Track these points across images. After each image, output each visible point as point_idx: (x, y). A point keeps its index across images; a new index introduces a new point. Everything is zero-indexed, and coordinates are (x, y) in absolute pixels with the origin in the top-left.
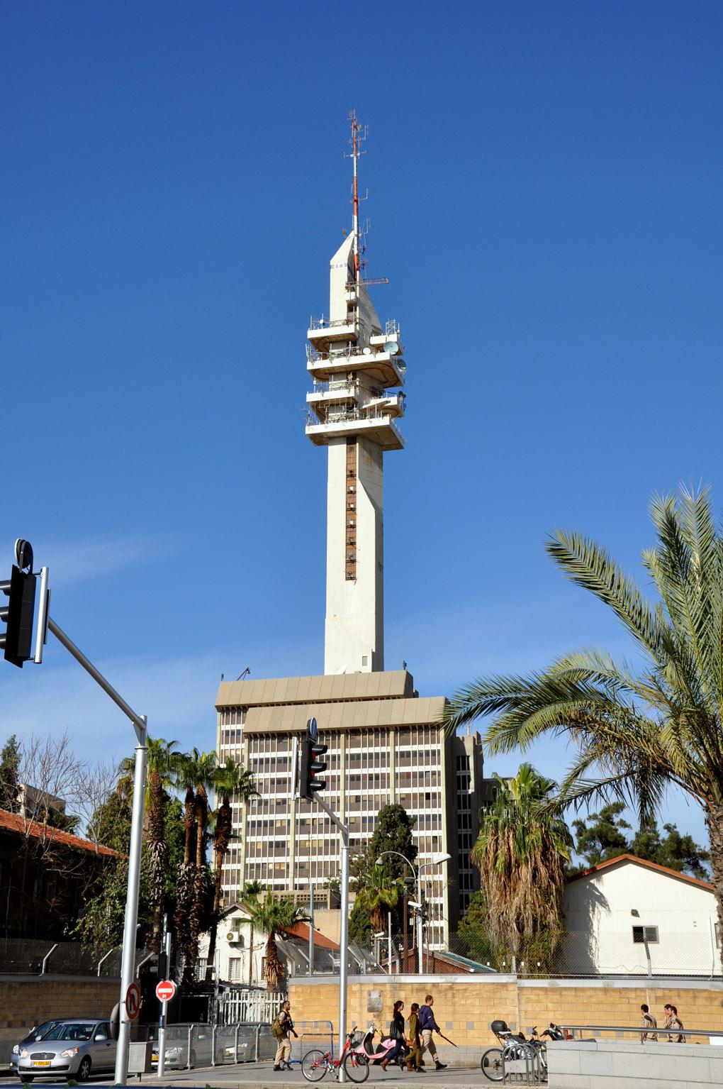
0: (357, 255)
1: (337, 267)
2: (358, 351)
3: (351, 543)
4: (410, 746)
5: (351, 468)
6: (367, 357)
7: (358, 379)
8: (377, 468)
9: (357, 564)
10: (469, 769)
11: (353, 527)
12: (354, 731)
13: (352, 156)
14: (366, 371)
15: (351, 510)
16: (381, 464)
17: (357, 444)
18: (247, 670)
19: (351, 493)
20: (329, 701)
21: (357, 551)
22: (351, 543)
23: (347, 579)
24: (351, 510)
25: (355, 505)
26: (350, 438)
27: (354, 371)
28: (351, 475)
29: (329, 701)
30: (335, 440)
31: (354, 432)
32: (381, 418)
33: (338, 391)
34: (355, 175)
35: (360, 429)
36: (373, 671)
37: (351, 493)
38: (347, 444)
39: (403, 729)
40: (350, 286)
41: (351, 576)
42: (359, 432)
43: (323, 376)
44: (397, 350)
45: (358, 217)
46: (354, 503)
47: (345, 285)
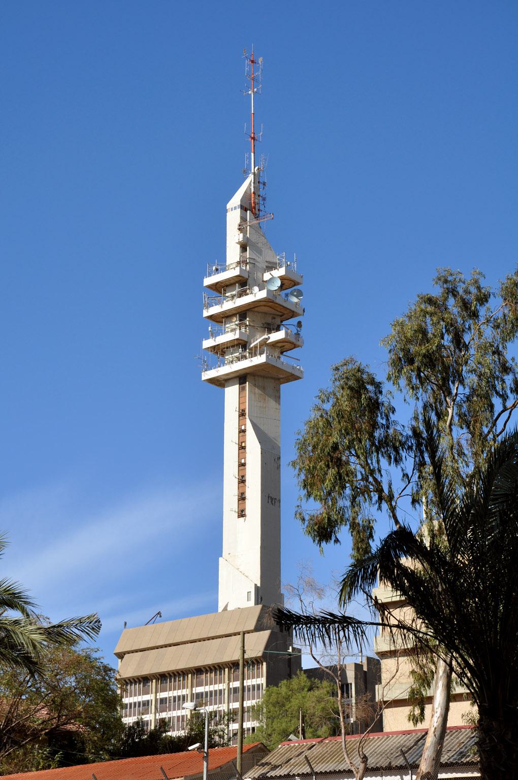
0: (254, 193)
1: (232, 210)
2: (248, 291)
3: (242, 481)
4: (203, 688)
5: (242, 408)
6: (257, 294)
7: (248, 319)
8: (272, 403)
9: (247, 501)
10: (352, 697)
11: (244, 465)
12: (198, 671)
13: (250, 92)
14: (256, 309)
15: (242, 448)
16: (277, 398)
17: (247, 383)
18: (158, 614)
19: (242, 432)
20: (200, 640)
21: (247, 488)
22: (242, 481)
23: (239, 517)
24: (242, 448)
25: (245, 444)
26: (241, 378)
27: (242, 313)
28: (242, 414)
29: (200, 640)
30: (230, 381)
31: (242, 373)
32: (259, 356)
33: (230, 334)
34: (253, 112)
35: (245, 369)
36: (255, 605)
37: (242, 432)
38: (240, 385)
39: (163, 677)
40: (241, 229)
41: (242, 514)
42: (247, 371)
43: (218, 320)
44: (279, 285)
45: (254, 153)
46: (245, 442)
47: (237, 227)
